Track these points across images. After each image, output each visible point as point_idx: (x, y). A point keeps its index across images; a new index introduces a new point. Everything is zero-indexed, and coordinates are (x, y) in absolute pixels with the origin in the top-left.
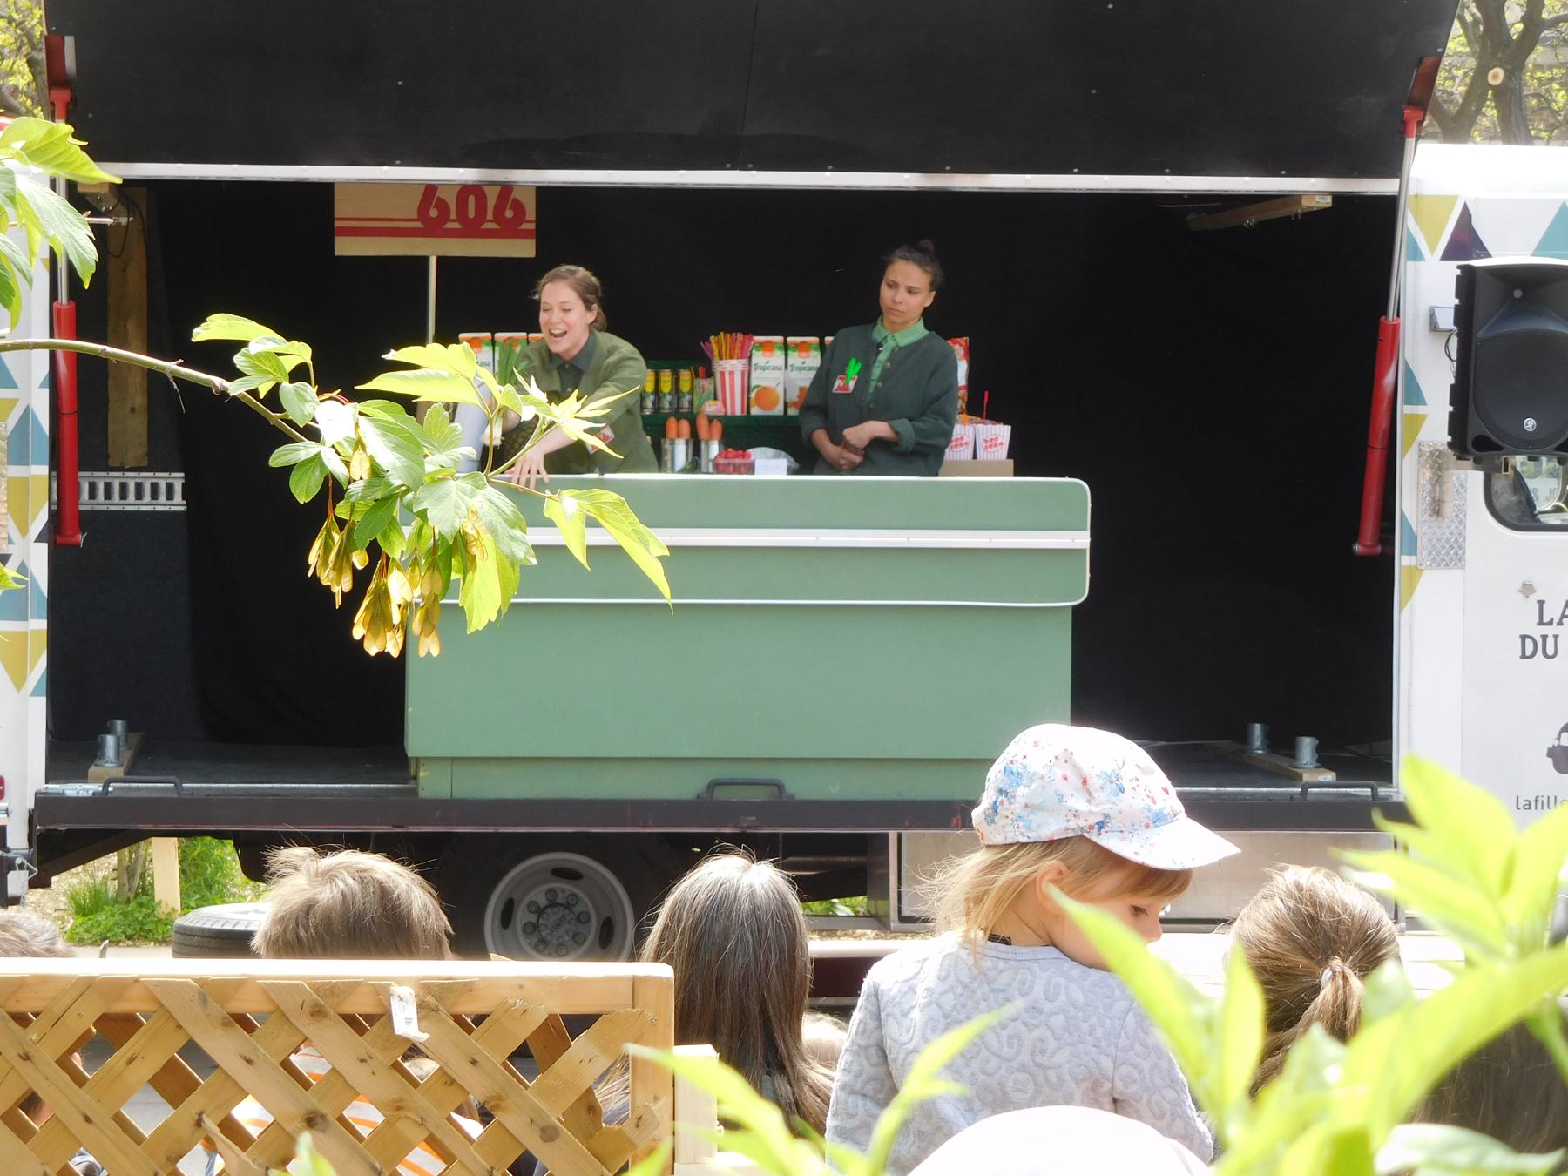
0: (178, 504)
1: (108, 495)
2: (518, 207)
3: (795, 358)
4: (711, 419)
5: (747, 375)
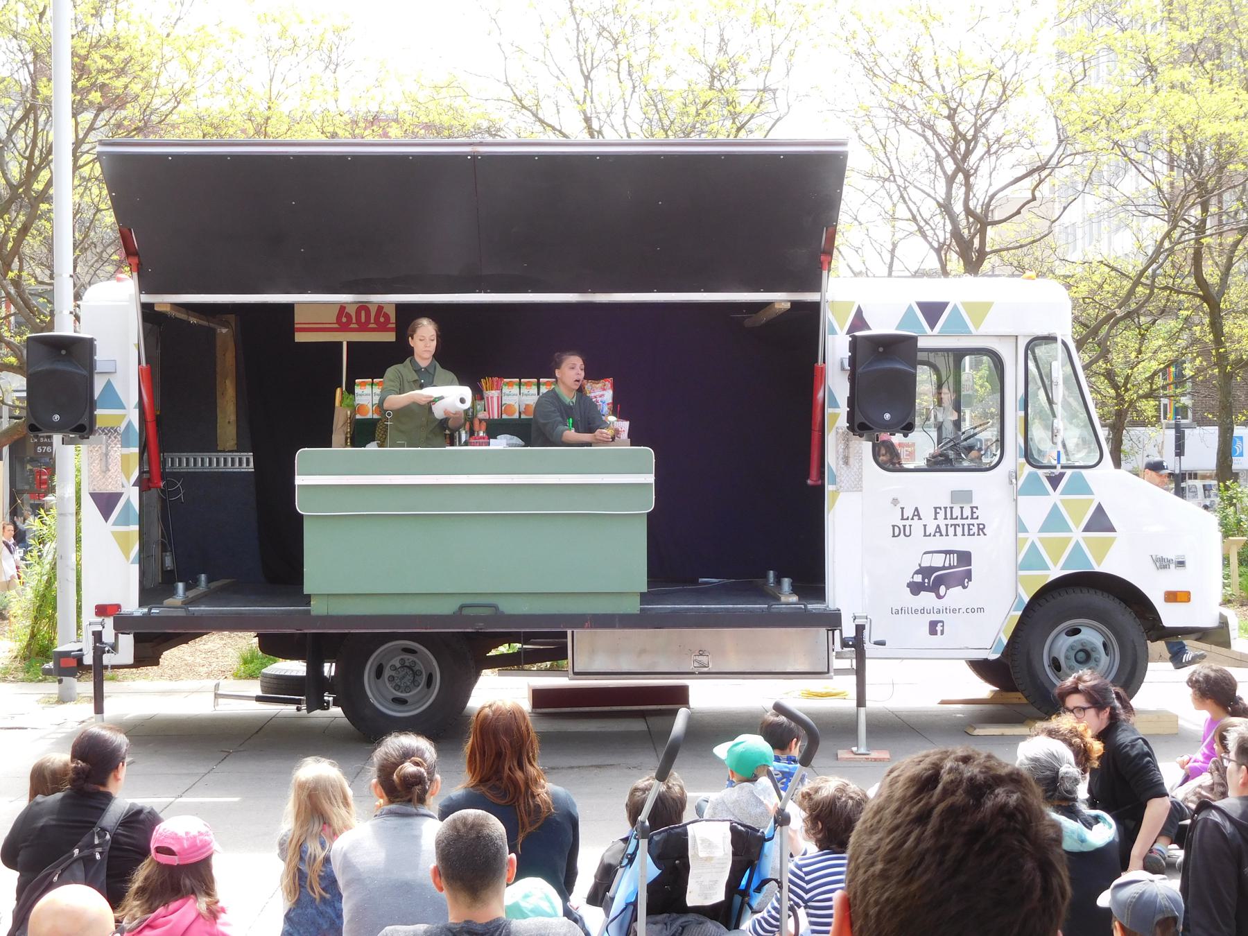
0: (251, 468)
1: (240, 464)
2: (387, 316)
3: (524, 390)
4: (480, 421)
5: (500, 399)
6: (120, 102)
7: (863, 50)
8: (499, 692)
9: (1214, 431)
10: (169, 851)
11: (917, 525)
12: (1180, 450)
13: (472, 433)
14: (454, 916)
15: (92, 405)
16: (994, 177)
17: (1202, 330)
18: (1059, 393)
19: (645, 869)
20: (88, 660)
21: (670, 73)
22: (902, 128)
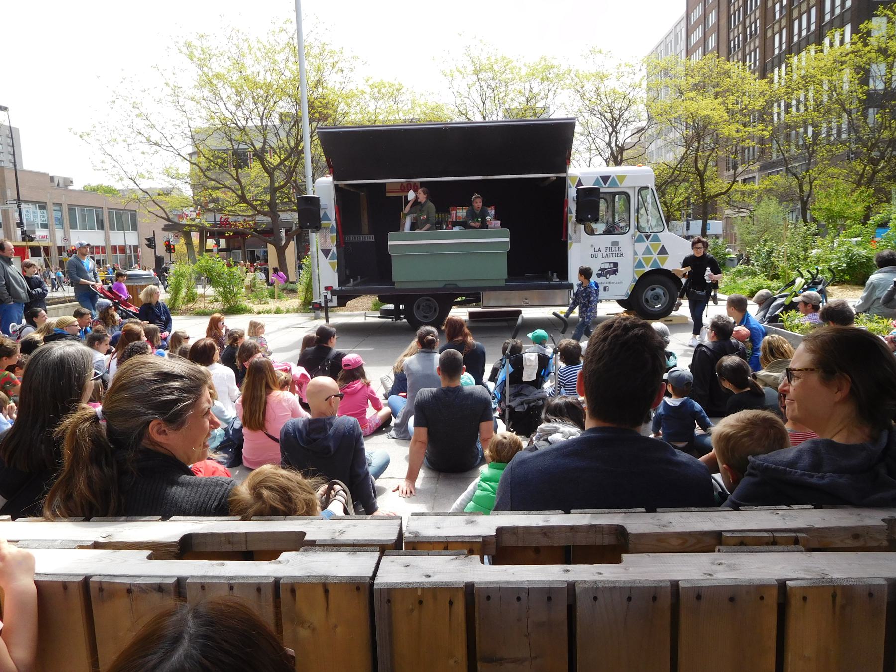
6: (325, 118)
7: (580, 89)
8: (460, 313)
9: (701, 221)
10: (348, 365)
11: (600, 254)
12: (688, 229)
13: (447, 226)
14: (443, 385)
15: (319, 219)
16: (625, 135)
17: (697, 186)
18: (650, 207)
19: (508, 369)
20: (323, 305)
21: (513, 100)
22: (593, 117)
